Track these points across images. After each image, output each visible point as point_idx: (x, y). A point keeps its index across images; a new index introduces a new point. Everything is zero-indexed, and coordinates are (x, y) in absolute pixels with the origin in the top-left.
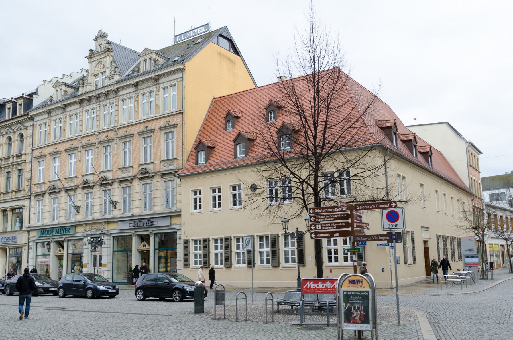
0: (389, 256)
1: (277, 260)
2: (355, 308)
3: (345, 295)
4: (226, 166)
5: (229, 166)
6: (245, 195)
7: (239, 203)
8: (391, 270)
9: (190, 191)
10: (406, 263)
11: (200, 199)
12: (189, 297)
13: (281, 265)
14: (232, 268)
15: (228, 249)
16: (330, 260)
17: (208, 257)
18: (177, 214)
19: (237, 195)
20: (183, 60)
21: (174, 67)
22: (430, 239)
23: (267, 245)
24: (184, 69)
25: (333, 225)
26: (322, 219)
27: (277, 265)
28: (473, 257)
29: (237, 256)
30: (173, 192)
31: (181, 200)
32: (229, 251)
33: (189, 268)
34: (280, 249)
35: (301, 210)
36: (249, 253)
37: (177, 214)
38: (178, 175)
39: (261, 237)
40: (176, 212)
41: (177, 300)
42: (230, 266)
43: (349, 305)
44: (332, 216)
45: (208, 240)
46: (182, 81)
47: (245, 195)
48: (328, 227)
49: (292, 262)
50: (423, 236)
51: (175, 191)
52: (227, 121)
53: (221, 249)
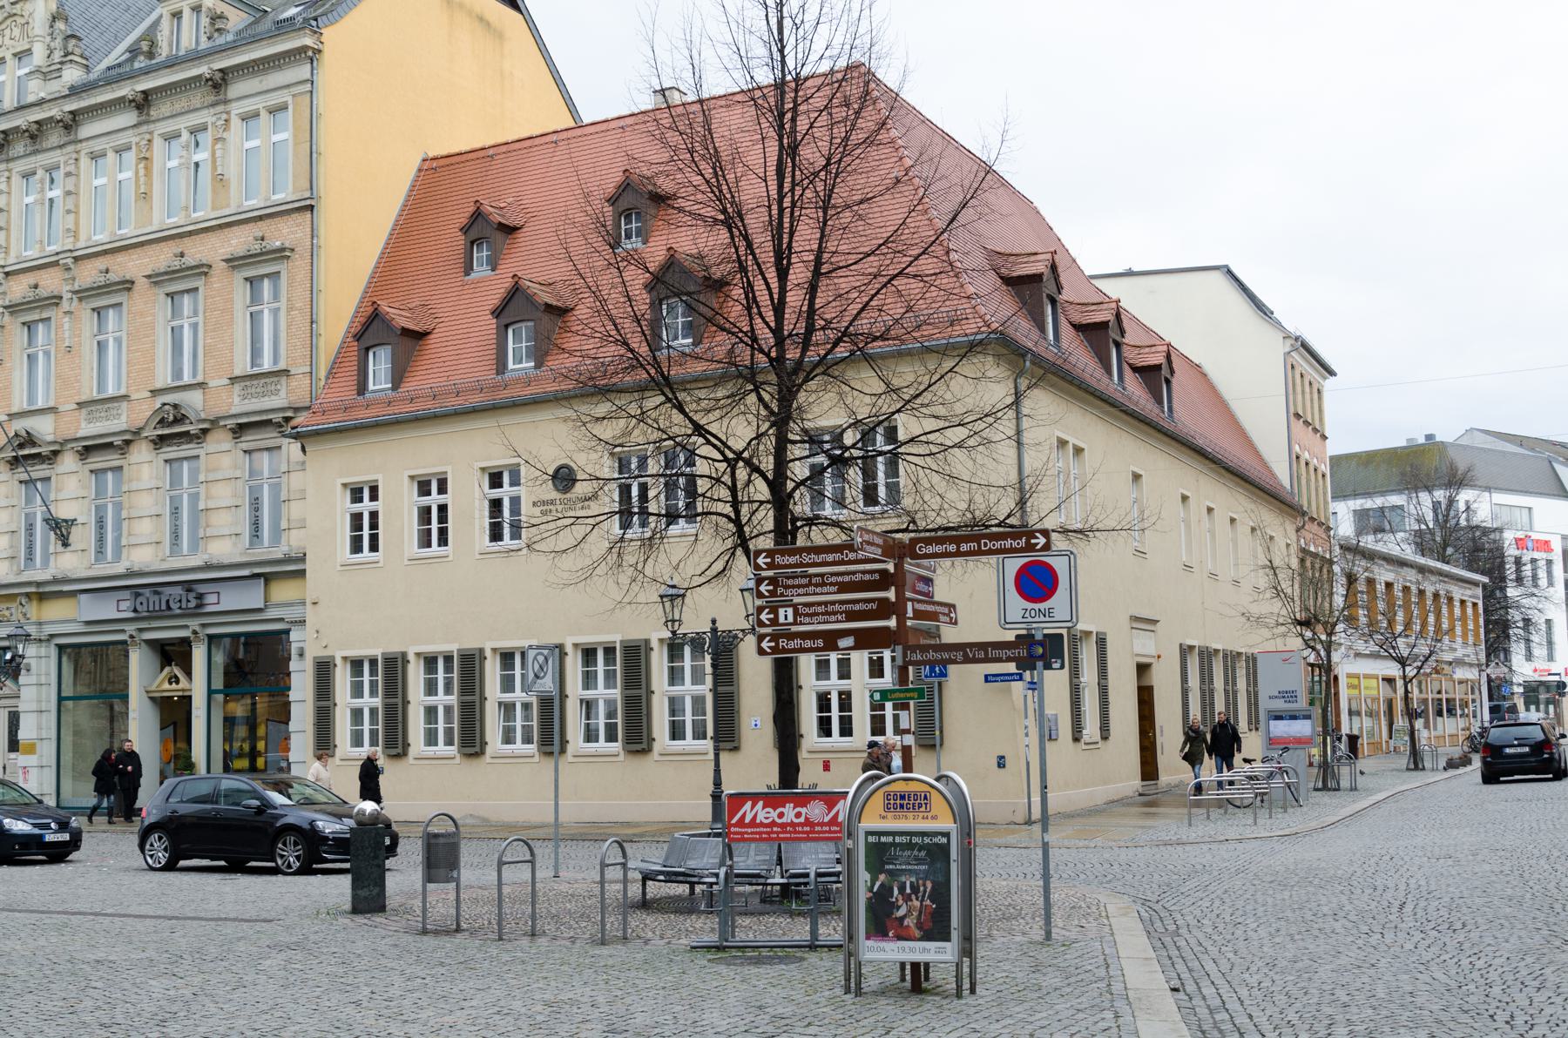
2: (902, 889)
4: (466, 400)
5: (476, 399)
6: (534, 504)
8: (1028, 763)
10: (1076, 739)
13: (657, 747)
14: (487, 758)
15: (472, 693)
16: (825, 728)
17: (400, 719)
18: (292, 569)
20: (316, 20)
22: (1159, 657)
23: (610, 676)
26: (799, 586)
28: (1294, 718)
31: (304, 520)
32: (476, 698)
34: (653, 692)
35: (726, 558)
36: (546, 703)
37: (292, 569)
38: (293, 428)
40: (288, 560)
41: (289, 866)
42: (477, 749)
43: (882, 877)
44: (833, 579)
46: (311, 92)
47: (534, 504)
48: (818, 614)
50: (1138, 650)
51: (284, 487)
52: (472, 243)
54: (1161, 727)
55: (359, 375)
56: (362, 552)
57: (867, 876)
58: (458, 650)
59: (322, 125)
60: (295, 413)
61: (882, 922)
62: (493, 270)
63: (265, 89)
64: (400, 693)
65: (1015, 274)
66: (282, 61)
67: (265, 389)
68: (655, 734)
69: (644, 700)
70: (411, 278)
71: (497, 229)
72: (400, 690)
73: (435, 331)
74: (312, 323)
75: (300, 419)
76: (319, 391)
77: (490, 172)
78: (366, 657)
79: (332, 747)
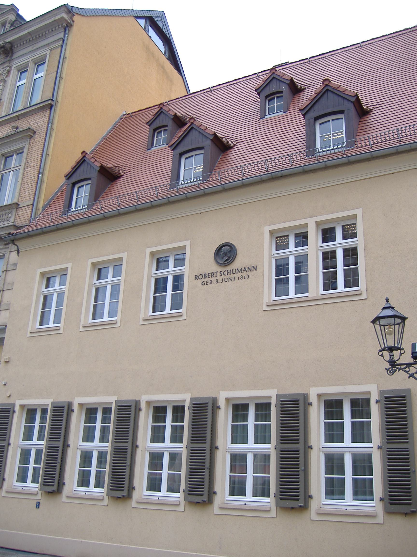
1: (302, 487)
6: (196, 277)
14: (133, 503)
17: (128, 462)
32: (129, 445)
34: (311, 448)
39: (91, 409)
42: (125, 493)
45: (133, 408)
47: (196, 277)
49: (170, 489)
64: (62, 437)
68: (136, 484)
69: (301, 455)
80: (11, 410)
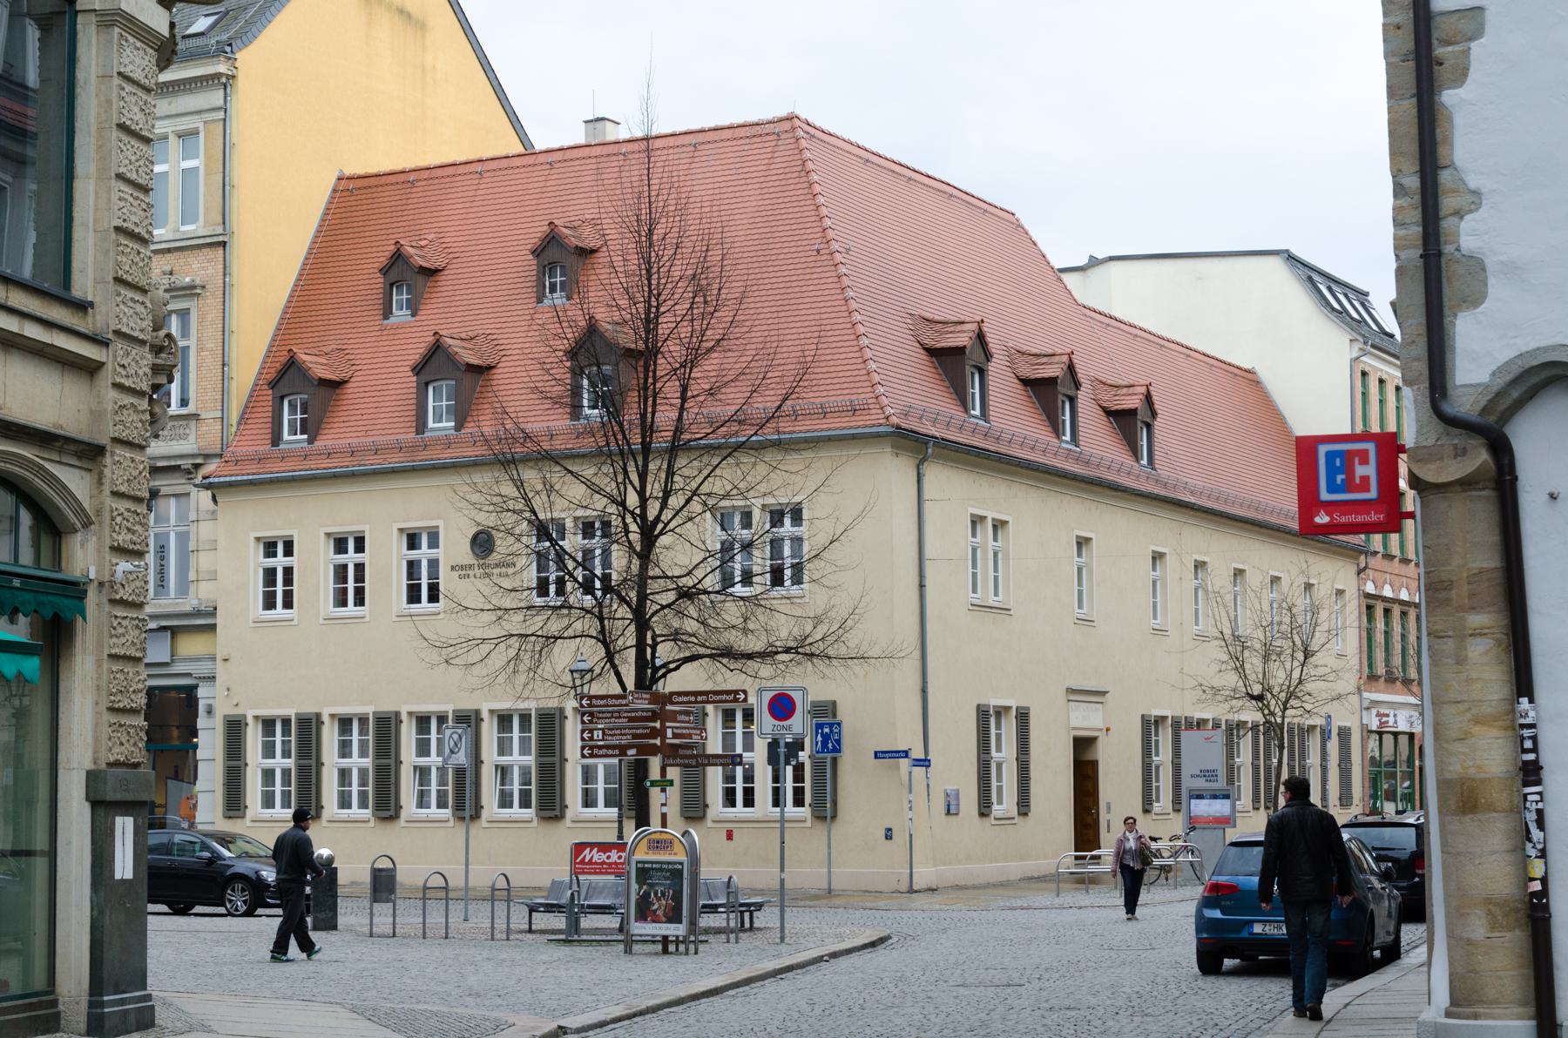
0: (908, 790)
2: (656, 894)
3: (637, 869)
4: (385, 459)
5: (395, 460)
6: (453, 568)
7: (429, 543)
8: (911, 836)
9: (252, 542)
10: (982, 815)
11: (288, 572)
12: (273, 901)
13: (569, 814)
14: (568, 822)
15: (388, 756)
16: (729, 797)
17: (314, 780)
18: (203, 623)
19: (424, 564)
20: (230, 45)
21: (196, 66)
22: (1108, 730)
23: (524, 743)
24: (234, 77)
25: (627, 731)
26: (606, 718)
27: (557, 813)
28: (1215, 797)
29: (420, 779)
30: (183, 538)
31: (216, 571)
32: (392, 761)
33: (243, 817)
34: (566, 760)
35: (602, 665)
36: (460, 773)
37: (203, 623)
38: (204, 478)
40: (197, 613)
41: (237, 910)
42: (392, 813)
43: (645, 887)
44: (626, 715)
45: (314, 721)
46: (225, 120)
47: (453, 568)
48: (615, 735)
50: (1074, 723)
51: (193, 537)
52: (392, 285)
53: (363, 754)
54: (1108, 805)
55: (273, 423)
56: (275, 608)
57: (637, 887)
58: (374, 713)
59: (235, 157)
60: (205, 459)
61: (644, 912)
62: (413, 315)
63: (174, 112)
65: (939, 345)
66: (193, 85)
67: (173, 432)
68: (568, 801)
69: (557, 768)
70: (326, 317)
71: (418, 272)
72: (314, 751)
73: (353, 380)
74: (223, 365)
75: (211, 467)
76: (231, 438)
77: (410, 201)
78: (278, 716)
79: (242, 808)
80: (243, 722)
